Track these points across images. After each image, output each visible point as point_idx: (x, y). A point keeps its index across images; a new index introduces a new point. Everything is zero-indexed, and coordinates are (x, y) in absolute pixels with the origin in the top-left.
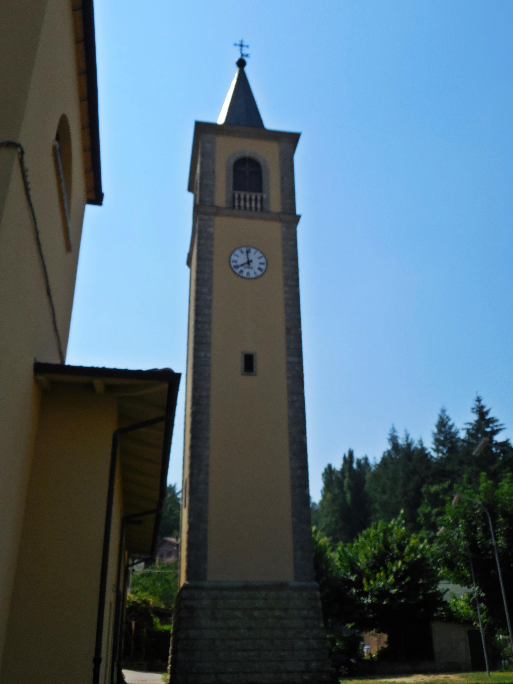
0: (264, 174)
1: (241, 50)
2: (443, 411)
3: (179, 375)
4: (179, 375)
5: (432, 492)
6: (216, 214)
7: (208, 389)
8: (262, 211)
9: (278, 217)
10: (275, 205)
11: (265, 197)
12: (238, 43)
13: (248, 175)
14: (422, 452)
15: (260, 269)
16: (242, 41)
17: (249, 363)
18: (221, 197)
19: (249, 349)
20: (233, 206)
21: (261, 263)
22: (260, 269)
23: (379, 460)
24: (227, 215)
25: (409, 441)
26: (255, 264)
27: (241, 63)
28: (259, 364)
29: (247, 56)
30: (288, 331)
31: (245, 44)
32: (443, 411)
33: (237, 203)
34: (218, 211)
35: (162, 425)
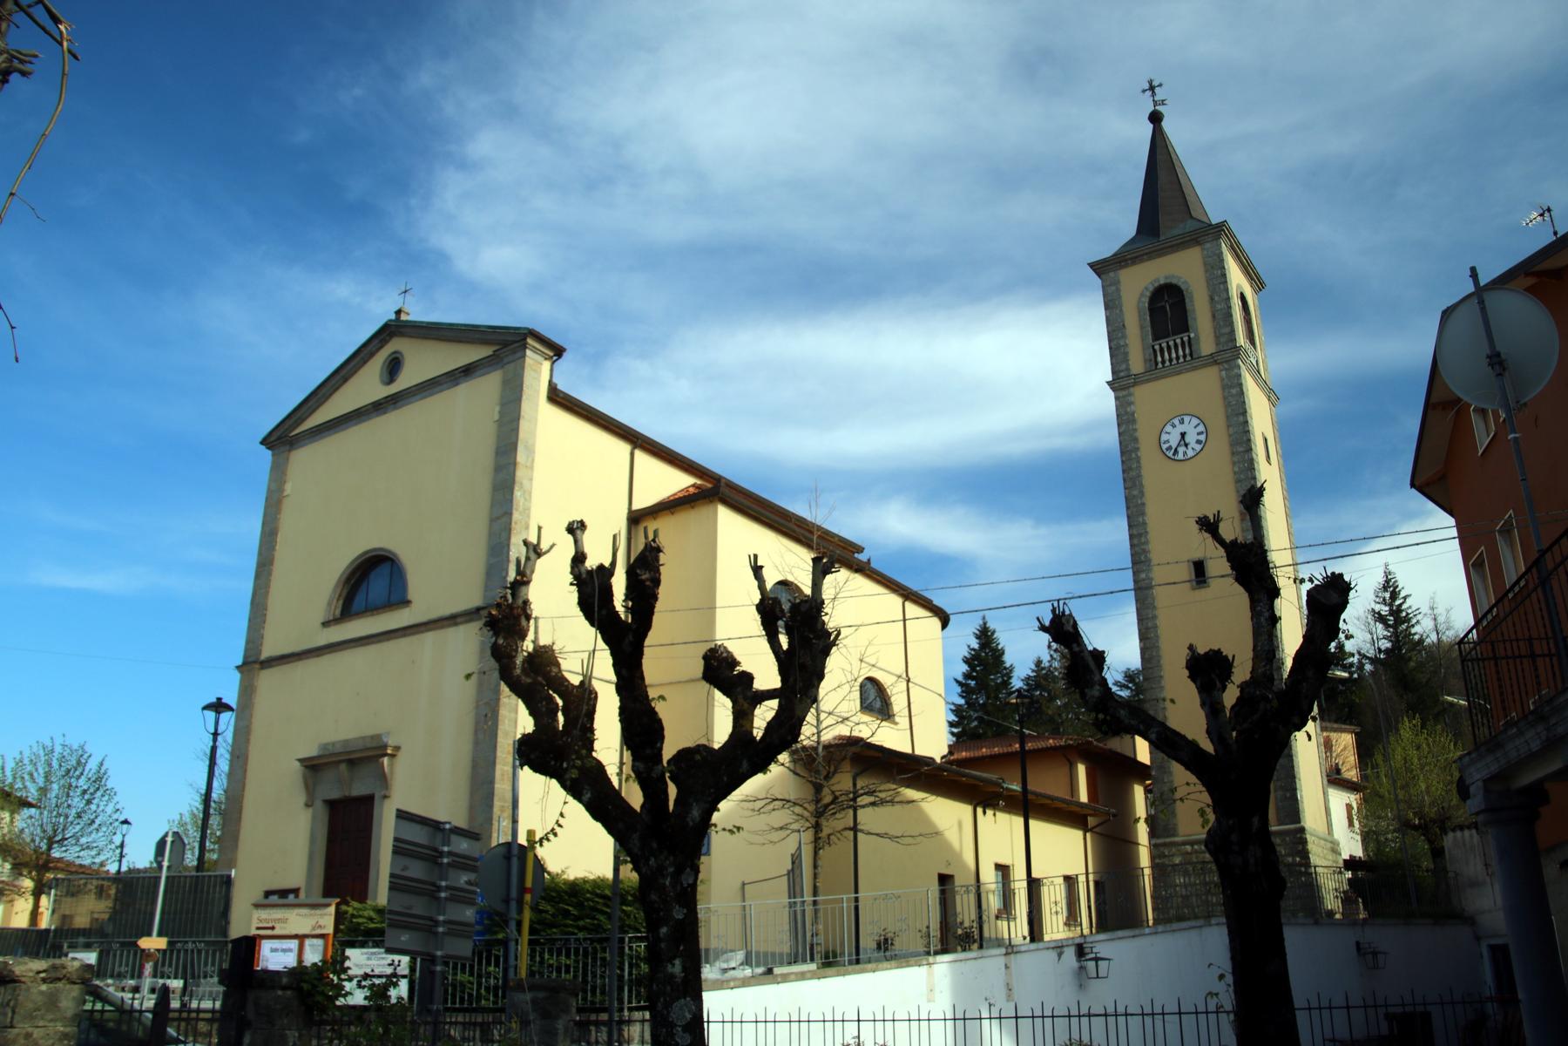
2: (1386, 565)
3: (405, 603)
4: (405, 603)
6: (1135, 384)
7: (1155, 617)
8: (1193, 359)
9: (1213, 360)
10: (1207, 346)
12: (1147, 86)
13: (1169, 309)
14: (1008, 673)
15: (1199, 442)
16: (1150, 82)
18: (1137, 364)
20: (1155, 369)
21: (1174, 426)
22: (1199, 442)
23: (572, 878)
24: (1148, 381)
25: (771, 579)
27: (1155, 118)
29: (1163, 102)
31: (1155, 83)
32: (1386, 565)
34: (1138, 380)
35: (1433, 400)
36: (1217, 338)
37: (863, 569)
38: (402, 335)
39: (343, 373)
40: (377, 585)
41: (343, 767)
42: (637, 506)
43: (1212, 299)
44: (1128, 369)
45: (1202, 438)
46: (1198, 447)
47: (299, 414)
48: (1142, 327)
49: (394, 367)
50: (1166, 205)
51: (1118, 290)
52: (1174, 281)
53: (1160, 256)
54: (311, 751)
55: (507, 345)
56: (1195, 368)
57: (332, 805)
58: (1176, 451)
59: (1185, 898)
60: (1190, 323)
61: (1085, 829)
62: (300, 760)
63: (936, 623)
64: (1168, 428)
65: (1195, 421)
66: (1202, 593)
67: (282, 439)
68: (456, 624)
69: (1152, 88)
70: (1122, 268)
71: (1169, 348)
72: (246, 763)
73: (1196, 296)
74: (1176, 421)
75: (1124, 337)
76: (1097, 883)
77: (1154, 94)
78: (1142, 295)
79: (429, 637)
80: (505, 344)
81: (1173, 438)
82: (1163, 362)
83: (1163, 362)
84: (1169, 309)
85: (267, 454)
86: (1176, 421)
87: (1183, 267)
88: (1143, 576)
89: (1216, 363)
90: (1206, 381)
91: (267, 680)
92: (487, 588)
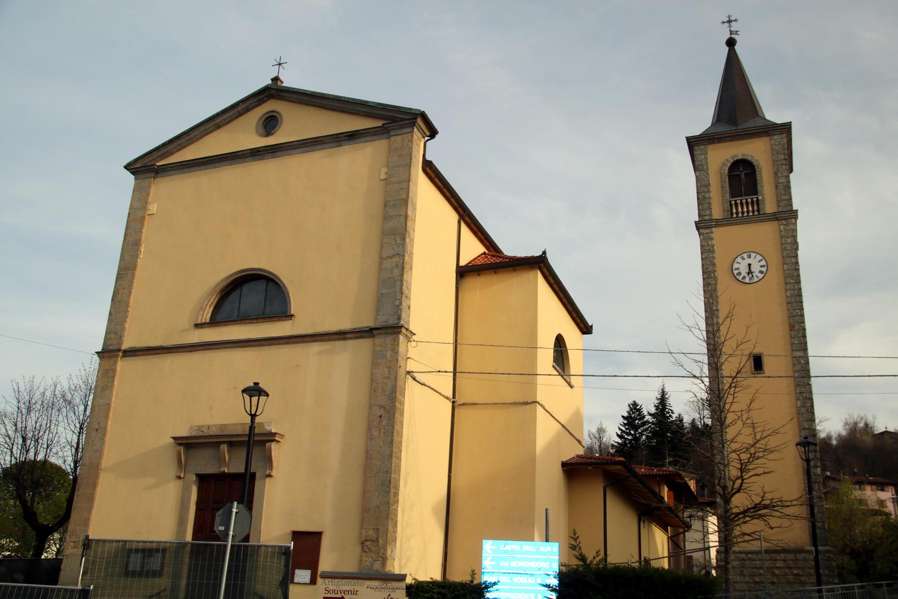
0: (757, 173)
1: (730, 26)
5: (484, 541)
8: (760, 216)
9: (775, 217)
10: (769, 207)
11: (760, 198)
12: (732, 18)
13: (742, 178)
15: (761, 272)
17: (758, 363)
18: (717, 212)
20: (730, 220)
21: (762, 266)
22: (761, 272)
26: (756, 268)
27: (731, 43)
28: (767, 362)
29: (736, 33)
30: (792, 328)
33: (734, 211)
34: (719, 223)
36: (778, 201)
38: (281, 98)
39: (218, 121)
40: (252, 296)
41: (224, 447)
42: (463, 263)
43: (776, 174)
44: (711, 215)
45: (764, 269)
46: (761, 276)
47: (169, 148)
48: (723, 187)
49: (270, 124)
50: (736, 104)
51: (706, 158)
52: (749, 158)
53: (731, 140)
54: (184, 432)
55: (399, 122)
56: (761, 221)
57: (203, 480)
58: (744, 278)
60: (759, 188)
62: (174, 438)
64: (739, 260)
67: (145, 168)
68: (345, 339)
69: (729, 22)
70: (710, 143)
71: (747, 203)
72: (104, 435)
73: (763, 172)
75: (709, 191)
77: (730, 26)
78: (724, 164)
79: (315, 348)
80: (393, 120)
81: (744, 270)
82: (737, 213)
83: (737, 213)
84: (742, 178)
85: (130, 178)
86: (745, 256)
87: (756, 150)
89: (777, 219)
90: (766, 232)
91: (122, 365)
92: (378, 311)
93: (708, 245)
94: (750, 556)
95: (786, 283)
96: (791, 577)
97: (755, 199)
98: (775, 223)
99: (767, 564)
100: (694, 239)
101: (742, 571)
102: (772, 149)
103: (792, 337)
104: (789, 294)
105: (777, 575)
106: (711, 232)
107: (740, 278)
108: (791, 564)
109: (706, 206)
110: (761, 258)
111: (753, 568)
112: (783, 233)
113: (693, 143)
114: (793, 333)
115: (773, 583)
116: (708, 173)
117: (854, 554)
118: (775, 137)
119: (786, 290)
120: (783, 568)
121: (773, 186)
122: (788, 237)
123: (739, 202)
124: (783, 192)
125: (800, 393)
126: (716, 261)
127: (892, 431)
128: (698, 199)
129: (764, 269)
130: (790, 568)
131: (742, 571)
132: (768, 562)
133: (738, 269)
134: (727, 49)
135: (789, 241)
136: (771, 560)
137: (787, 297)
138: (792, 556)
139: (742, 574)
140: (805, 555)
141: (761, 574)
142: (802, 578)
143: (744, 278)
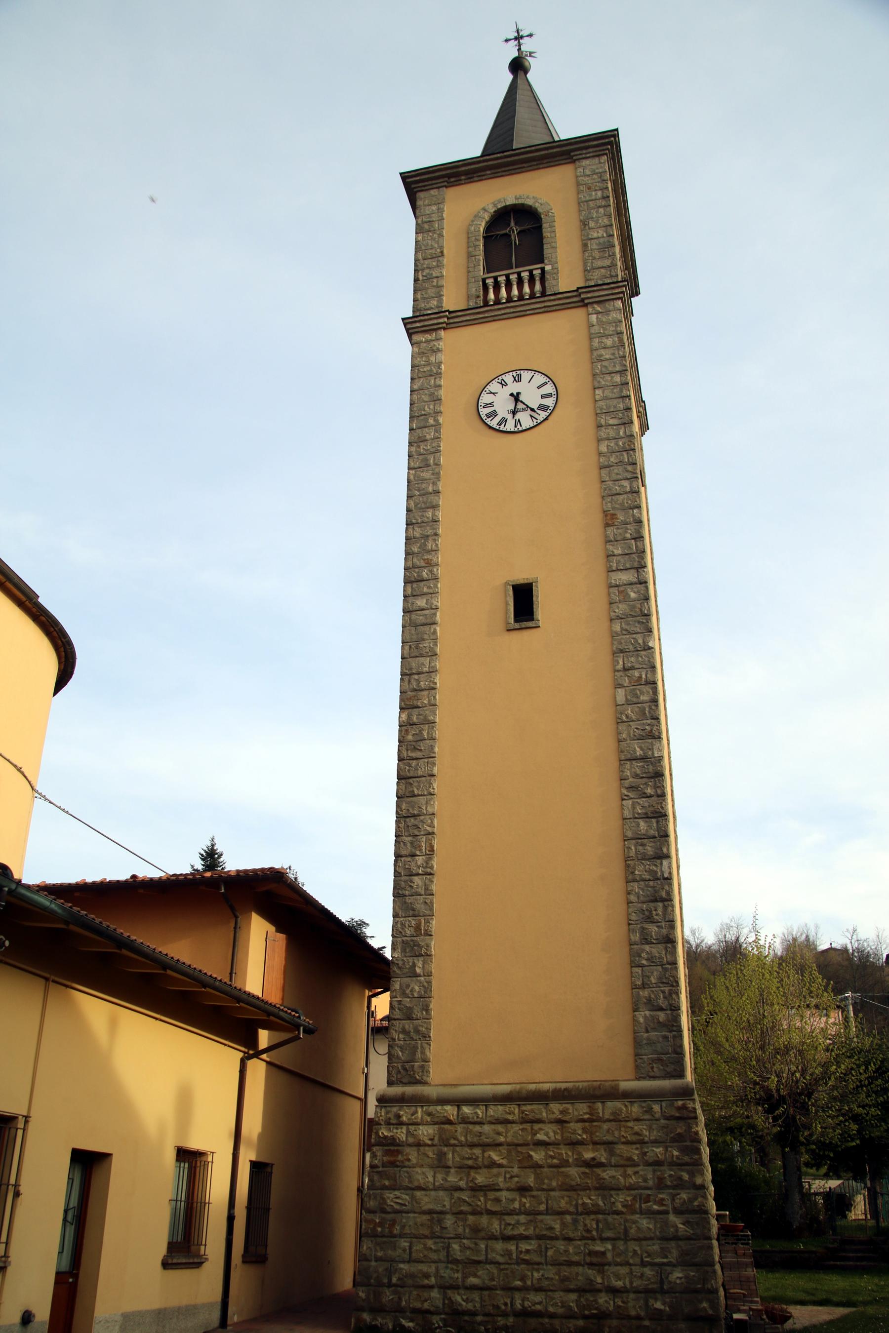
8: (545, 300)
9: (579, 299)
11: (548, 268)
13: (515, 236)
17: (524, 602)
19: (521, 577)
20: (482, 311)
21: (503, 384)
26: (532, 398)
27: (518, 66)
34: (454, 320)
37: (615, 701)
43: (584, 224)
45: (550, 402)
48: (470, 256)
51: (440, 211)
52: (529, 202)
56: (547, 310)
58: (504, 421)
59: (435, 1215)
61: (251, 1050)
63: (47, 661)
64: (494, 387)
65: (540, 379)
66: (526, 638)
69: (518, 38)
74: (508, 378)
75: (440, 266)
76: (255, 1166)
81: (502, 405)
84: (515, 236)
86: (508, 378)
87: (547, 190)
88: (421, 602)
90: (557, 335)
93: (429, 364)
94: (466, 1110)
95: (599, 426)
96: (573, 1172)
97: (537, 273)
98: (578, 314)
99: (514, 1133)
100: (400, 351)
101: (441, 1156)
102: (578, 184)
103: (608, 541)
104: (603, 448)
105: (537, 1166)
106: (438, 339)
107: (494, 423)
108: (577, 1130)
109: (431, 292)
110: (543, 379)
111: (472, 1145)
112: (595, 329)
113: (417, 183)
114: (610, 531)
115: (523, 1190)
116: (441, 235)
117: (770, 1102)
118: (585, 162)
119: (599, 440)
120: (555, 1144)
121: (577, 245)
122: (607, 336)
123: (502, 279)
124: (597, 254)
125: (625, 669)
126: (442, 393)
127: (839, 947)
128: (416, 280)
129: (550, 402)
130: (573, 1144)
131: (441, 1156)
132: (516, 1128)
133: (491, 404)
134: (510, 77)
135: (609, 342)
136: (524, 1121)
137: (600, 454)
138: (582, 1109)
139: (441, 1164)
140: (618, 1104)
141: (493, 1164)
142: (607, 1174)
143: (504, 421)
